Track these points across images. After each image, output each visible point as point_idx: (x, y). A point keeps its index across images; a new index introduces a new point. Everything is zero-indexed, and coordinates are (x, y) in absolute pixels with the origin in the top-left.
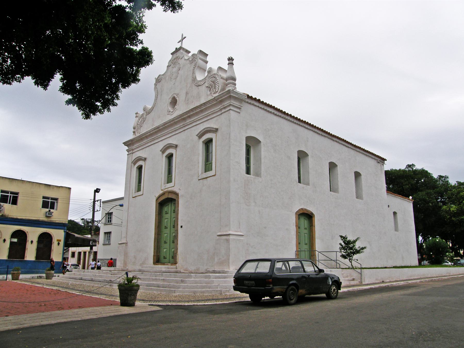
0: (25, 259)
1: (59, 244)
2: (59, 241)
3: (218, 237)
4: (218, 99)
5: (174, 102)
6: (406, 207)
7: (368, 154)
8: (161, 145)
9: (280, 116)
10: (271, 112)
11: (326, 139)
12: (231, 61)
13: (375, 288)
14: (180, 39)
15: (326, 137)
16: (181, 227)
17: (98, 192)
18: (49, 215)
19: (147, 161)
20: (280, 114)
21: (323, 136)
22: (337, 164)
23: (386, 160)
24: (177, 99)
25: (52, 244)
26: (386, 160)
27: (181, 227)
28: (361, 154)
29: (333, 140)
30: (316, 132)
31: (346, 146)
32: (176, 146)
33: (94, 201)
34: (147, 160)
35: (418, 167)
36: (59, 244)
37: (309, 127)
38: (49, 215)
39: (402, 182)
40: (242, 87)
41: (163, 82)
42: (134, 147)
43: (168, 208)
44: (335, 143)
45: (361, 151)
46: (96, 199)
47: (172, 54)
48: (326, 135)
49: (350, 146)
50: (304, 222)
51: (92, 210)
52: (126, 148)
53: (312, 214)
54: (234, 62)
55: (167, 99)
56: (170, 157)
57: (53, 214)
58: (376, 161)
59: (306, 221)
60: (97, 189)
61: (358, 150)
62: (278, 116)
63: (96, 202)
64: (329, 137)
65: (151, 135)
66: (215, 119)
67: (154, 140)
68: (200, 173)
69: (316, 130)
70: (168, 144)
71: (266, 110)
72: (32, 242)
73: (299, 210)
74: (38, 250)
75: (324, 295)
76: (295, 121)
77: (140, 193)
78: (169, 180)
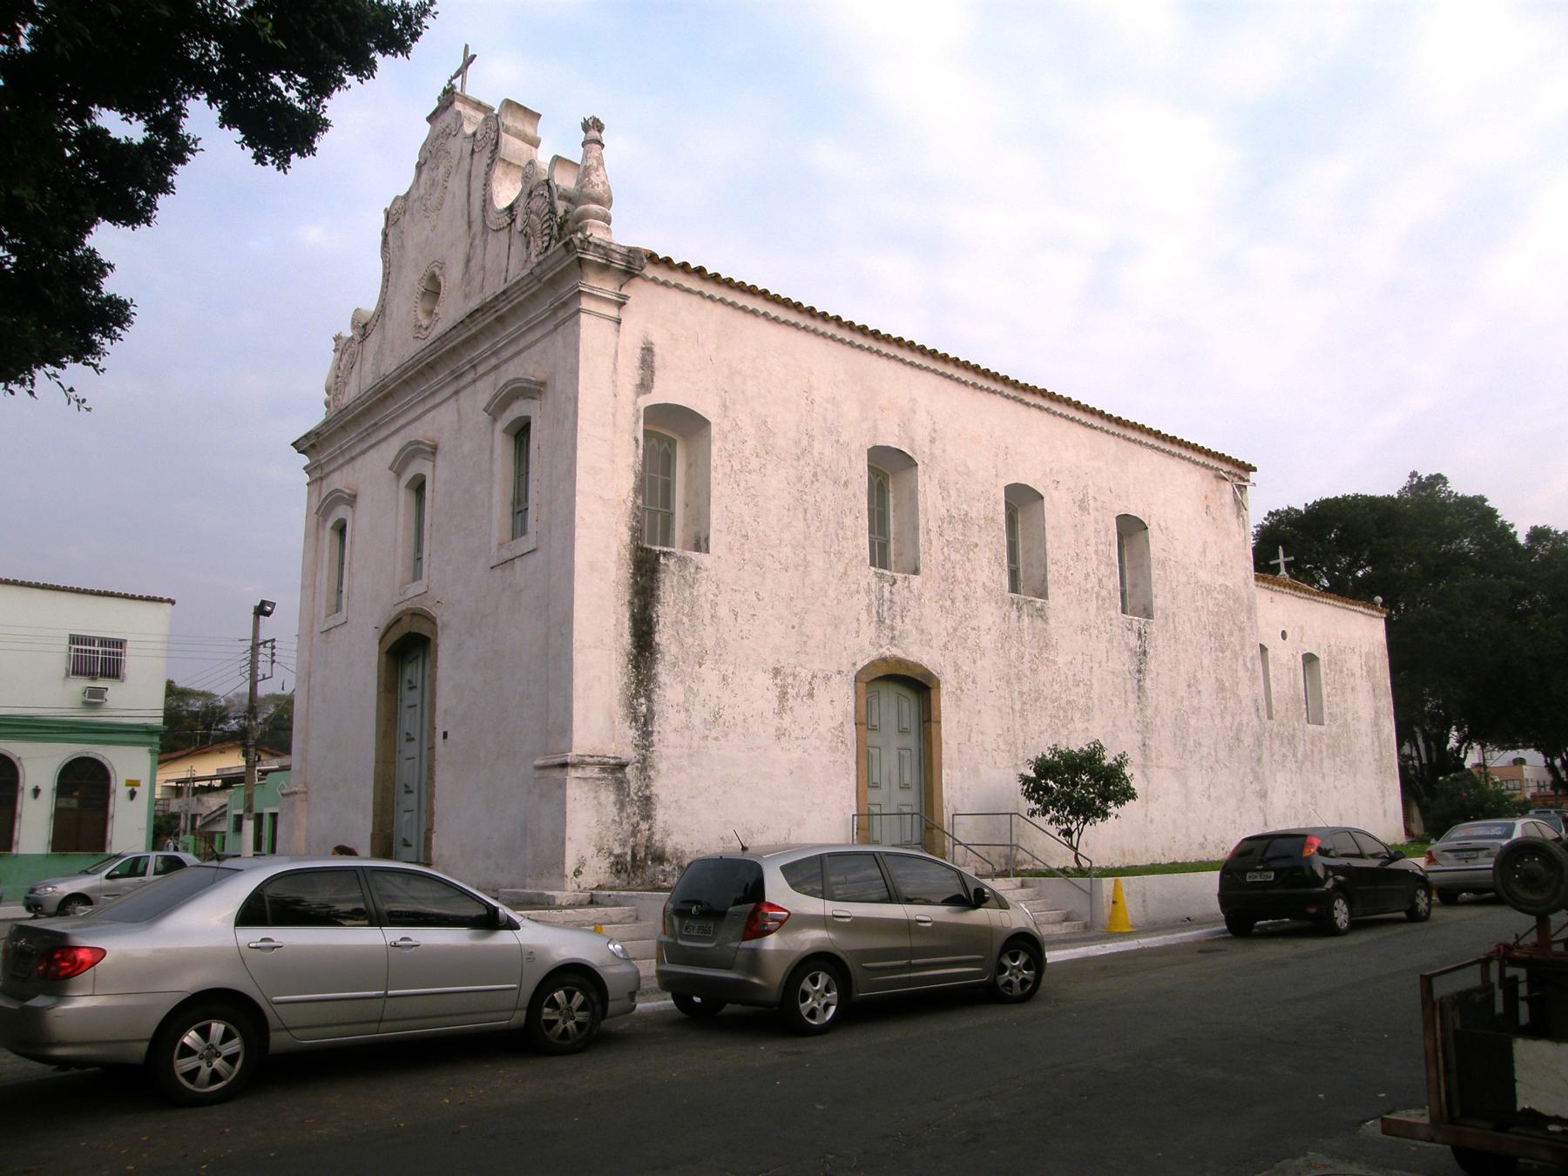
0: (14, 851)
1: (133, 794)
2: (133, 784)
3: (537, 774)
4: (544, 273)
5: (432, 290)
6: (1356, 637)
7: (1175, 449)
8: (392, 448)
9: (795, 325)
10: (754, 312)
11: (996, 399)
12: (594, 134)
13: (1178, 945)
14: (460, 63)
15: (994, 392)
16: (445, 735)
17: (268, 614)
18: (94, 698)
19: (362, 503)
20: (793, 317)
21: (981, 388)
22: (1041, 491)
23: (1255, 469)
24: (441, 279)
25: (108, 797)
26: (1255, 469)
27: (445, 735)
28: (1147, 452)
29: (1027, 404)
30: (950, 377)
31: (1084, 424)
32: (434, 450)
33: (255, 647)
34: (359, 499)
35: (1461, 485)
36: (133, 794)
37: (918, 359)
38: (94, 698)
39: (1316, 547)
40: (626, 229)
41: (405, 221)
42: (323, 457)
43: (411, 672)
44: (1035, 413)
45: (1144, 438)
46: (263, 636)
47: (429, 119)
48: (998, 387)
49: (1097, 422)
50: (895, 706)
51: (247, 675)
52: (305, 460)
53: (929, 675)
54: (605, 137)
55: (411, 280)
56: (418, 487)
57: (107, 695)
58: (1211, 474)
59: (905, 705)
60: (263, 603)
61: (1134, 435)
62: (786, 323)
63: (261, 649)
64: (1009, 391)
65: (368, 411)
66: (539, 346)
67: (377, 427)
68: (494, 543)
69: (950, 370)
70: (410, 443)
71: (733, 305)
72: (36, 792)
73: (872, 664)
74: (60, 816)
75: (1403, 915)
76: (859, 339)
77: (341, 618)
78: (417, 575)
